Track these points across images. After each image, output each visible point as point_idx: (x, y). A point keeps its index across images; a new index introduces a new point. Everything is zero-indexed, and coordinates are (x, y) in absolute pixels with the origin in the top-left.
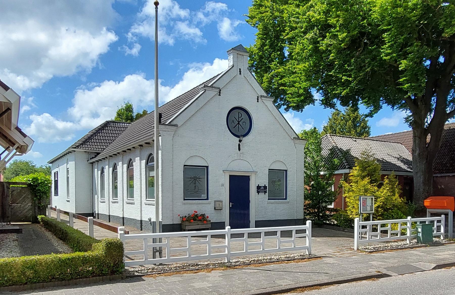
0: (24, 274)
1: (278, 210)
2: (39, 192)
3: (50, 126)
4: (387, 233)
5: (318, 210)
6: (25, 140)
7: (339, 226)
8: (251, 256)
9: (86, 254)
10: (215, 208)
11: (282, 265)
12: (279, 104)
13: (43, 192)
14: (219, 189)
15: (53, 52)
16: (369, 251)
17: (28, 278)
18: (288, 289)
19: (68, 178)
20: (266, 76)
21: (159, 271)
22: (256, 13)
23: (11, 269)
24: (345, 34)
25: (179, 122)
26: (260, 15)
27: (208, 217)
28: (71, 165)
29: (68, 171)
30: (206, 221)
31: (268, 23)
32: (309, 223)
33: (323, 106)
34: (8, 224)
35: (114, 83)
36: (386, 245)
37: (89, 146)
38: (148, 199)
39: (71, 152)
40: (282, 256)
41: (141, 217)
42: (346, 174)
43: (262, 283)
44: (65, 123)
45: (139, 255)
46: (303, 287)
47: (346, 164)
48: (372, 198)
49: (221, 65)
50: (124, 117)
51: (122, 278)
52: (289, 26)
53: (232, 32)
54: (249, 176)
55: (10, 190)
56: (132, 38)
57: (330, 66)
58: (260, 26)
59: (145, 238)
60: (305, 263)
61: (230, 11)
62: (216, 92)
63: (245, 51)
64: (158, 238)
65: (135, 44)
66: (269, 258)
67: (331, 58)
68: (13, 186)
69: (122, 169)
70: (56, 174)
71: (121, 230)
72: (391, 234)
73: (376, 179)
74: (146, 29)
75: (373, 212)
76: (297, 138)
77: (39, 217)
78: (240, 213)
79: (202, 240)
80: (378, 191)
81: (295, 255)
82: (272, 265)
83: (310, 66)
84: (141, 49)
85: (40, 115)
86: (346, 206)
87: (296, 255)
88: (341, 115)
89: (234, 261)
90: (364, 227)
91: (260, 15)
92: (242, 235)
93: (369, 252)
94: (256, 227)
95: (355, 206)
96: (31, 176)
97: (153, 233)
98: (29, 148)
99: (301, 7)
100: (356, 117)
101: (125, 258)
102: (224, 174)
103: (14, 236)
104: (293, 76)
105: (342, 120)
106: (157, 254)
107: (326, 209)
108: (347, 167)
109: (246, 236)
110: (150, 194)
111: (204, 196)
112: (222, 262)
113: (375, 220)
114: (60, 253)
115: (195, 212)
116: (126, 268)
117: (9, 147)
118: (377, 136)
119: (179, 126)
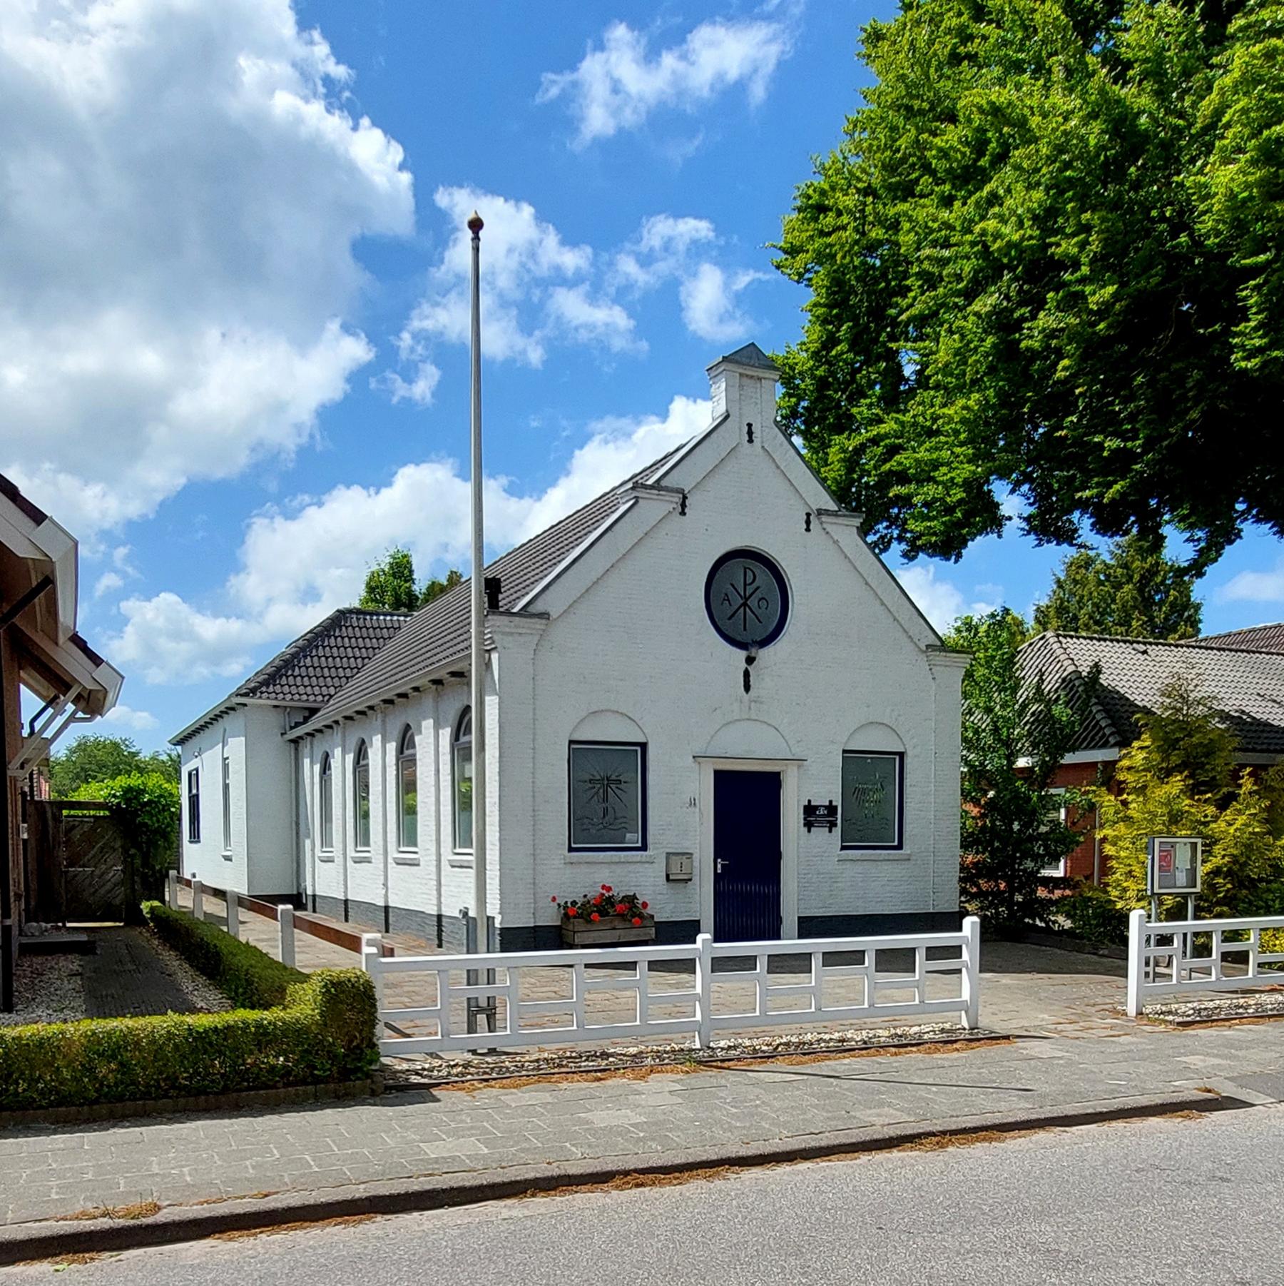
0: (89, 1069)
1: (872, 882)
2: (145, 829)
3: (178, 634)
4: (1246, 962)
5: (1009, 884)
6: (99, 673)
7: (1081, 937)
8: (777, 1030)
9: (266, 1016)
10: (668, 876)
11: (879, 1059)
12: (882, 537)
13: (156, 831)
14: (683, 817)
15: (185, 406)
16: (1180, 1019)
17: (102, 1085)
18: (891, 1139)
19: (226, 787)
20: (842, 444)
21: (485, 1073)
22: (805, 235)
23: (53, 1056)
24: (1111, 289)
25: (553, 604)
26: (819, 242)
27: (645, 905)
28: (236, 747)
29: (226, 767)
30: (641, 916)
31: (845, 266)
32: (970, 924)
33: (1032, 537)
34: (58, 928)
35: (365, 493)
36: (1242, 1001)
37: (286, 689)
38: (458, 850)
39: (233, 709)
40: (880, 1032)
41: (439, 904)
42: (1110, 765)
43: (809, 1116)
44: (222, 620)
45: (426, 1022)
46: (944, 1133)
47: (1107, 731)
48: (1194, 845)
49: (691, 418)
50: (388, 598)
51: (373, 1093)
52: (917, 274)
53: (727, 311)
54: (779, 774)
55: (63, 826)
56: (412, 350)
57: (1059, 402)
58: (821, 276)
59: (442, 969)
60: (955, 1055)
61: (722, 242)
62: (669, 503)
63: (769, 364)
64: (482, 968)
65: (420, 365)
66: (836, 1036)
67: (1060, 374)
68: (72, 812)
69: (382, 755)
70: (194, 776)
71: (370, 943)
72: (1260, 965)
73: (1214, 778)
74: (450, 319)
75: (1198, 889)
76: (942, 646)
77: (145, 906)
78: (748, 896)
79: (624, 976)
80: (1216, 819)
81: (925, 1028)
82: (846, 1061)
83: (986, 406)
84: (440, 382)
85: (149, 600)
86: (1106, 871)
87: (927, 1027)
88: (1099, 567)
89: (722, 1044)
90: (1165, 940)
91: (819, 242)
92: (747, 963)
93: (1179, 1024)
94: (800, 936)
95: (1137, 870)
96: (122, 781)
97: (468, 952)
98: (110, 696)
99: (957, 204)
100: (1153, 571)
101: (380, 1029)
102: (696, 766)
103: (73, 963)
104: (927, 445)
105: (1100, 583)
106: (482, 1018)
107: (1034, 880)
108: (1112, 740)
109: (761, 965)
110: (462, 835)
111: (634, 838)
112: (686, 1046)
113: (1204, 918)
114: (194, 1010)
115: (604, 887)
116: (385, 1060)
117: (56, 697)
118: (1223, 633)
119: (554, 615)
